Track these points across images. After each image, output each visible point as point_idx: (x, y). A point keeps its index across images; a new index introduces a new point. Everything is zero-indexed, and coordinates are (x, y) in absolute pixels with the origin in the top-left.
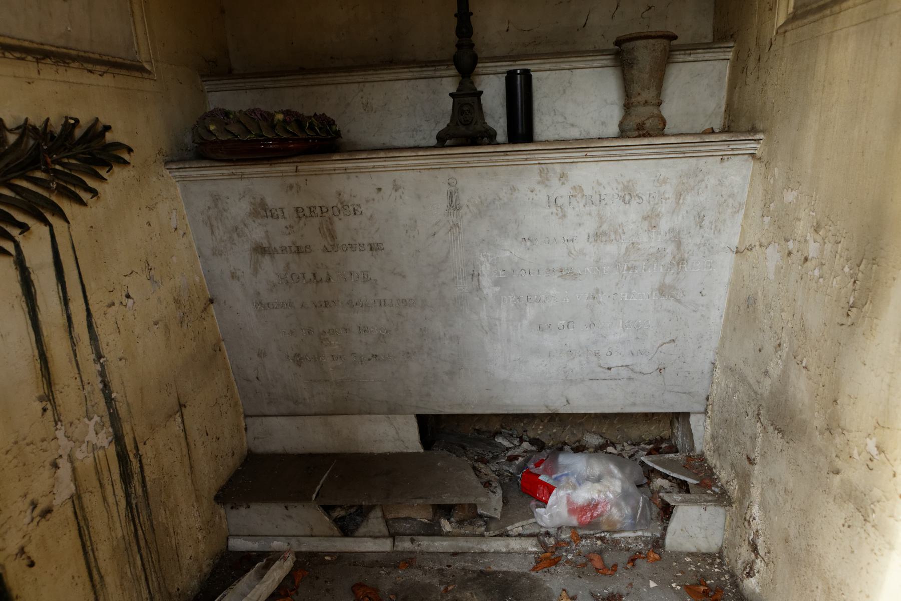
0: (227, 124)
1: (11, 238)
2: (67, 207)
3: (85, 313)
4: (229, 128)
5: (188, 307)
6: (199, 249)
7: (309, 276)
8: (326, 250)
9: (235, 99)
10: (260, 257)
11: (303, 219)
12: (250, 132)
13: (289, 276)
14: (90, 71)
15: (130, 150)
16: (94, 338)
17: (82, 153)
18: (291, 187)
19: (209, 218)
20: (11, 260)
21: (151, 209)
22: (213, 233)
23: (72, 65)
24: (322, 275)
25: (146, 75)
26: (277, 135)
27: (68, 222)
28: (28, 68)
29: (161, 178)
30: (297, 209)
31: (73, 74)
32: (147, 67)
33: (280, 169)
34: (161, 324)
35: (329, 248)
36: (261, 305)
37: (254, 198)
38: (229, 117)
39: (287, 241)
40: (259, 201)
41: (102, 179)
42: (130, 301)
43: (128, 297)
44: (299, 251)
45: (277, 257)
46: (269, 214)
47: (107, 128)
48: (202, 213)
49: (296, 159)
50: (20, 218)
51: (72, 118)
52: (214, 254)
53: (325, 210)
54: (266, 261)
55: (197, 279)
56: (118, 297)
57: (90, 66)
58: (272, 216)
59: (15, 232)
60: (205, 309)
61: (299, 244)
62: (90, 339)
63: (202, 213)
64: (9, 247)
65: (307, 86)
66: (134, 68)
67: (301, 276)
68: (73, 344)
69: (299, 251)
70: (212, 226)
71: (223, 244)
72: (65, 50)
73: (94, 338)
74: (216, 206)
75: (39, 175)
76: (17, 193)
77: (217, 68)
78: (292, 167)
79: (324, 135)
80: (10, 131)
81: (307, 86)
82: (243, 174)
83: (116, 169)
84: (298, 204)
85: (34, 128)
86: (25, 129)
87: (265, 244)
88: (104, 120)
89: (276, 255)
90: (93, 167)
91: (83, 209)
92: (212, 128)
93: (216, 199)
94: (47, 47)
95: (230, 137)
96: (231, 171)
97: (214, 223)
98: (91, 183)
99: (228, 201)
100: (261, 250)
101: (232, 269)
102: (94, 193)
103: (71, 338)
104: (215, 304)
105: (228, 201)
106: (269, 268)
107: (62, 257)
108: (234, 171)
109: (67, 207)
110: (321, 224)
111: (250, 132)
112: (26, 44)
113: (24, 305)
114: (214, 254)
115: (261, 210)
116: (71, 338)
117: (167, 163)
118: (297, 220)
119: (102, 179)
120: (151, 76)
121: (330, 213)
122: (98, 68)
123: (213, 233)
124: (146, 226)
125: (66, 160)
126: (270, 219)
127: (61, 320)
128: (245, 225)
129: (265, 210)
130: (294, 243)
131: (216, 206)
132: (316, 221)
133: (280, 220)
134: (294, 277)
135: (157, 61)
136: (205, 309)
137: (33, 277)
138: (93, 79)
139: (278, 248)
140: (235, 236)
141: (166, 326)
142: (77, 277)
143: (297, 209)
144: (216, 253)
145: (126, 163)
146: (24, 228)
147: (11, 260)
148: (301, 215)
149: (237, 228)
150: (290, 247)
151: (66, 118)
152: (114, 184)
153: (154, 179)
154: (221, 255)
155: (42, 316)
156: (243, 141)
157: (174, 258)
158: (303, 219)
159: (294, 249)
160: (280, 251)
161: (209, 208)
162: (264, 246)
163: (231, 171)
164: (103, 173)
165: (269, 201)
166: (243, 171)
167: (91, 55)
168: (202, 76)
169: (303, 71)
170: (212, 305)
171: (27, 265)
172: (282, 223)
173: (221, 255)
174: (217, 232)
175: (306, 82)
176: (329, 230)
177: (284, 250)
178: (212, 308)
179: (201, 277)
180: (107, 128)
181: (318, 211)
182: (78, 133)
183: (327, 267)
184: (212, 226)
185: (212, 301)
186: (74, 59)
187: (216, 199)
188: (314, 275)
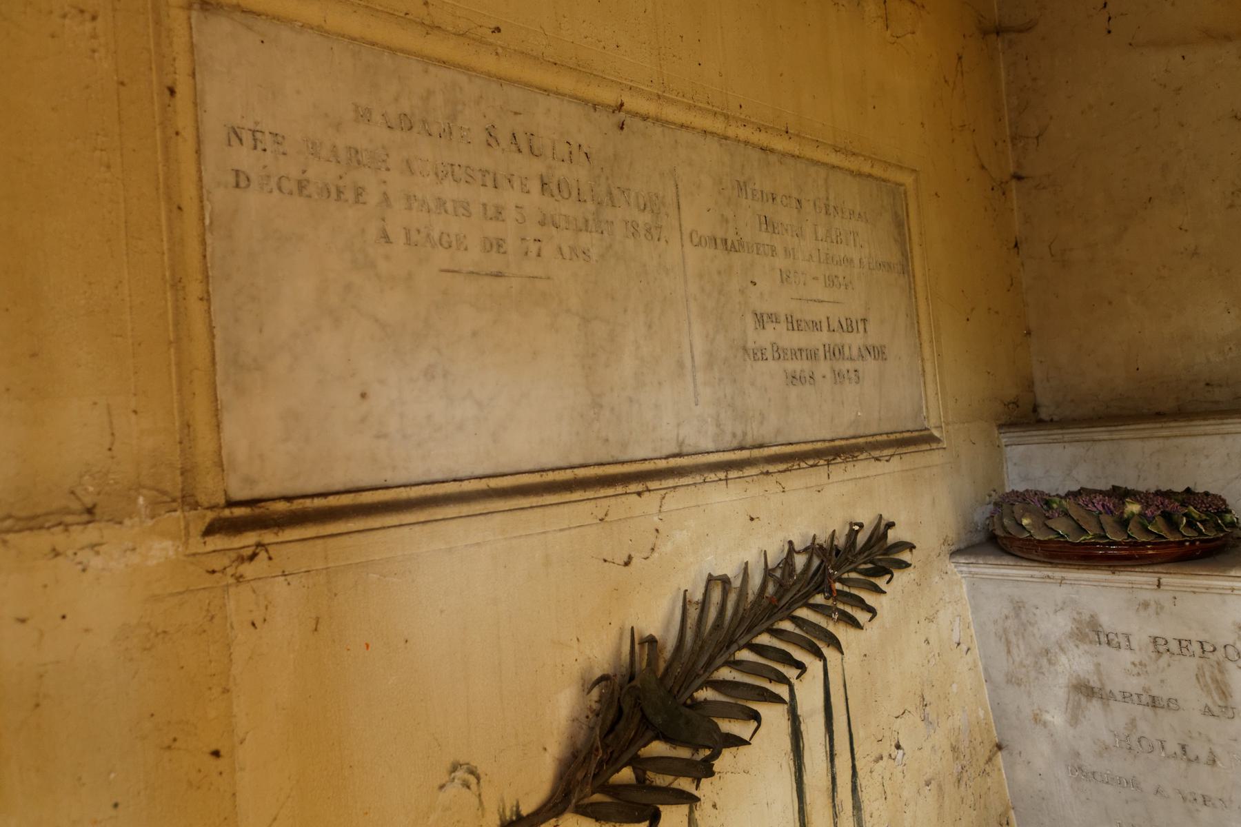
0: (1048, 518)
1: (783, 680)
2: (842, 633)
3: (850, 772)
4: (1051, 523)
5: (968, 757)
6: (985, 670)
7: (1173, 747)
8: (1208, 711)
9: (1049, 466)
10: (1084, 700)
11: (1166, 657)
12: (1085, 532)
13: (1134, 739)
14: (877, 459)
15: (912, 547)
16: (857, 807)
17: (865, 563)
18: (1146, 605)
19: (1005, 630)
20: (786, 707)
21: (930, 620)
22: (1009, 652)
23: (861, 457)
24: (1199, 749)
25: (934, 446)
26: (1129, 536)
27: (842, 653)
28: (815, 476)
29: (944, 576)
30: (1155, 640)
31: (863, 468)
32: (936, 433)
33: (1128, 578)
34: (934, 785)
35: (1216, 710)
36: (1079, 771)
37: (1079, 613)
38: (1050, 508)
39: (1134, 684)
40: (1086, 617)
41: (878, 590)
42: (901, 752)
43: (898, 747)
44: (1154, 703)
45: (1116, 706)
46: (1104, 639)
47: (891, 525)
48: (995, 622)
49: (1157, 569)
50: (798, 655)
51: (856, 524)
52: (1009, 681)
53: (1208, 648)
54: (1095, 706)
55: (981, 713)
56: (888, 748)
57: (877, 453)
58: (1109, 643)
59: (791, 673)
60: (990, 759)
61: (1155, 692)
62: (854, 808)
63: (995, 622)
64: (783, 691)
65: (1167, 437)
66: (919, 440)
67: (1157, 745)
68: (835, 815)
69: (1154, 703)
70: (1008, 643)
71: (1023, 670)
72: (853, 441)
73: (857, 807)
74: (1017, 616)
75: (819, 599)
76: (798, 625)
77: (1023, 415)
78: (1153, 579)
79: (1212, 535)
80: (799, 552)
81: (1167, 437)
82: (1063, 578)
83: (897, 574)
84: (1157, 633)
85: (821, 547)
86: (813, 549)
87: (1094, 682)
88: (887, 517)
89: (1112, 702)
90: (872, 580)
91: (858, 631)
92: (1025, 522)
93: (1018, 607)
94: (837, 443)
95: (1052, 537)
96: (1046, 573)
97: (1013, 639)
98: (870, 598)
99: (1037, 612)
100: (1085, 690)
101: (1035, 707)
102: (872, 611)
103: (834, 806)
104: (1005, 752)
105: (1037, 612)
106: (1100, 721)
107: (833, 699)
108: (1050, 574)
109: (842, 633)
110: (1200, 668)
111: (1085, 532)
112: (819, 445)
113: (792, 763)
114: (1009, 681)
115: (1090, 631)
116: (834, 806)
117: (953, 554)
118: (1154, 655)
119: (878, 590)
120: (940, 445)
121: (1220, 653)
122: (886, 452)
123: (1009, 652)
124: (924, 645)
125: (845, 576)
126: (1105, 648)
127: (825, 782)
128: (1062, 649)
129: (1098, 633)
130: (1144, 689)
131: (1017, 616)
132: (1192, 663)
133: (1122, 650)
134: (1144, 742)
135: (947, 424)
136: (990, 759)
137: (803, 727)
138: (881, 467)
139: (1116, 692)
140: (1044, 662)
141: (940, 787)
142: (846, 724)
143: (1155, 640)
144: (1013, 680)
145: (908, 565)
146: (801, 666)
147: (786, 707)
148: (1161, 649)
149: (1047, 651)
150: (1139, 695)
151: (851, 524)
152: (894, 596)
153: (937, 579)
154: (1019, 685)
155: (807, 778)
156: (1072, 543)
157: (955, 686)
158: (1166, 657)
159: (1145, 699)
160: (1119, 697)
161: (1007, 617)
162: (1092, 684)
163: (1046, 573)
164: (881, 582)
165: (1106, 621)
166: (1064, 575)
167: (879, 438)
168: (1000, 426)
169: (1159, 416)
170: (999, 754)
171: (799, 712)
172: (1126, 657)
173: (1019, 685)
174: (1015, 651)
175: (1165, 433)
176: (1216, 681)
177: (1126, 696)
178: (1000, 758)
179: (986, 713)
180: (891, 525)
181: (1196, 647)
182: (861, 539)
183: (1209, 740)
184: (1008, 643)
185: (999, 747)
186: (860, 449)
187: (1018, 607)
188: (1183, 747)
